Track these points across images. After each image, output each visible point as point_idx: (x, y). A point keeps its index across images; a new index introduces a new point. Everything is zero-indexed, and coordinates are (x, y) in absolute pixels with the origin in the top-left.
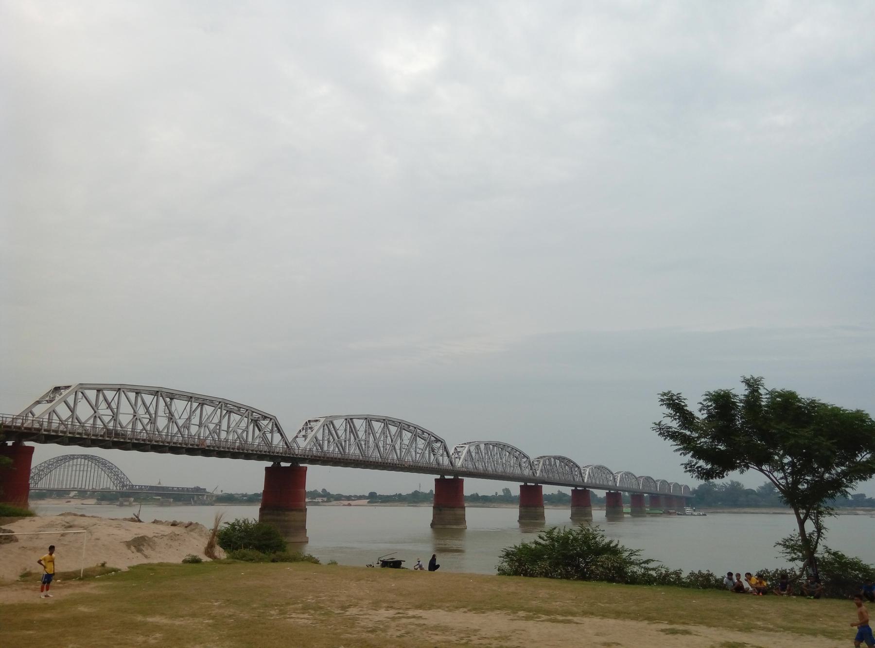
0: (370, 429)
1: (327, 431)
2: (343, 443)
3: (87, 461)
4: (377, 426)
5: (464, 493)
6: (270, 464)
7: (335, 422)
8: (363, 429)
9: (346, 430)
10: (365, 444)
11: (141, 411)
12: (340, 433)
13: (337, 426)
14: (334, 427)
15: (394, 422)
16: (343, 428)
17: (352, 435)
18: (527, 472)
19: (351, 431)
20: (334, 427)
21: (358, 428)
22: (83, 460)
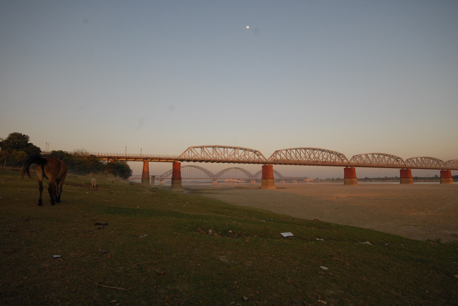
0: (373, 157)
1: (360, 158)
2: (365, 161)
3: (237, 170)
4: (423, 159)
5: (451, 174)
6: (263, 165)
7: (362, 156)
8: (371, 157)
9: (365, 158)
10: (372, 161)
11: (307, 154)
12: (364, 158)
13: (363, 157)
14: (362, 157)
15: (387, 155)
16: (364, 157)
17: (368, 159)
18: (442, 166)
19: (367, 158)
20: (362, 157)
21: (369, 157)
22: (235, 169)
